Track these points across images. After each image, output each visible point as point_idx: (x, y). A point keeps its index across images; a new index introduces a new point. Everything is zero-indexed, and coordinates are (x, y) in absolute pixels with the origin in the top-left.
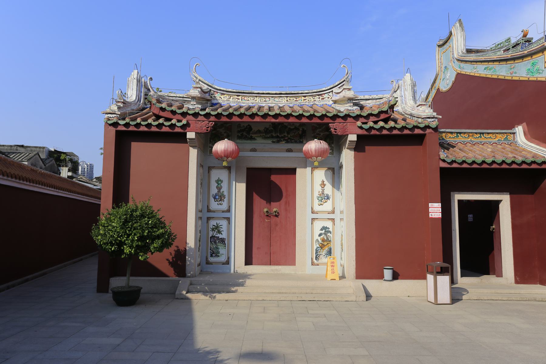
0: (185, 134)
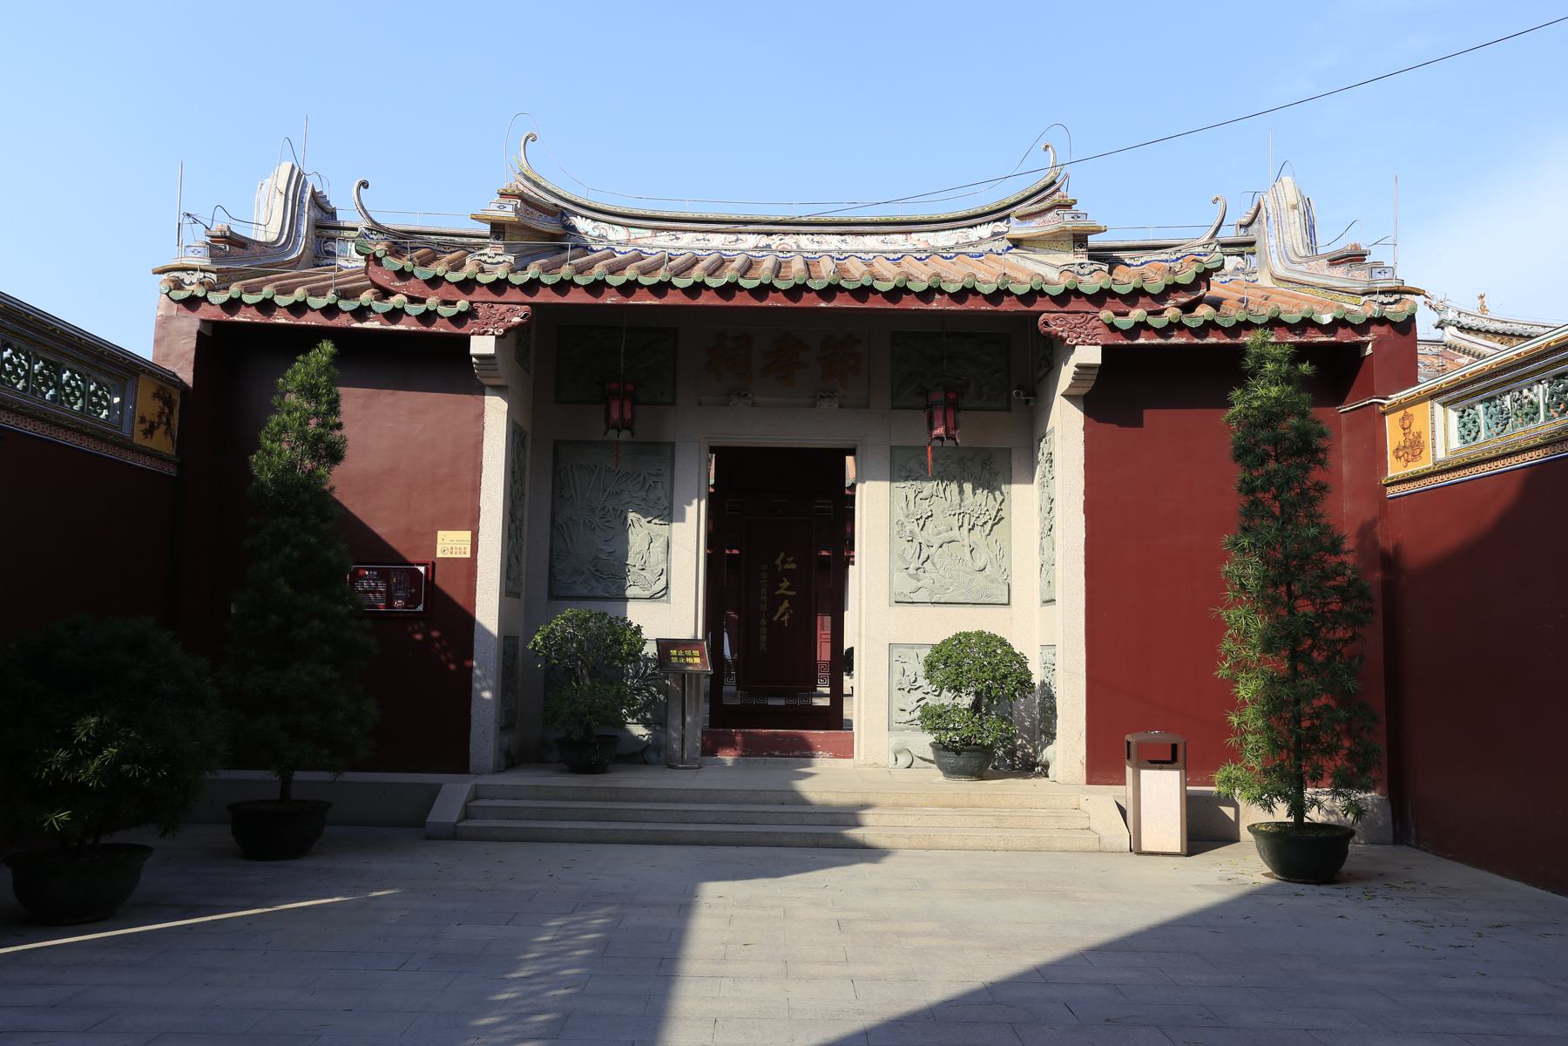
0: (465, 340)
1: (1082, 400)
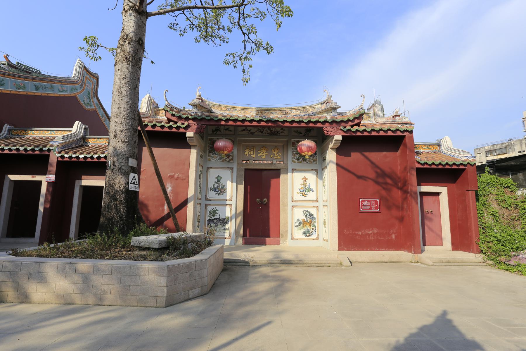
0: (185, 133)
1: (335, 150)
